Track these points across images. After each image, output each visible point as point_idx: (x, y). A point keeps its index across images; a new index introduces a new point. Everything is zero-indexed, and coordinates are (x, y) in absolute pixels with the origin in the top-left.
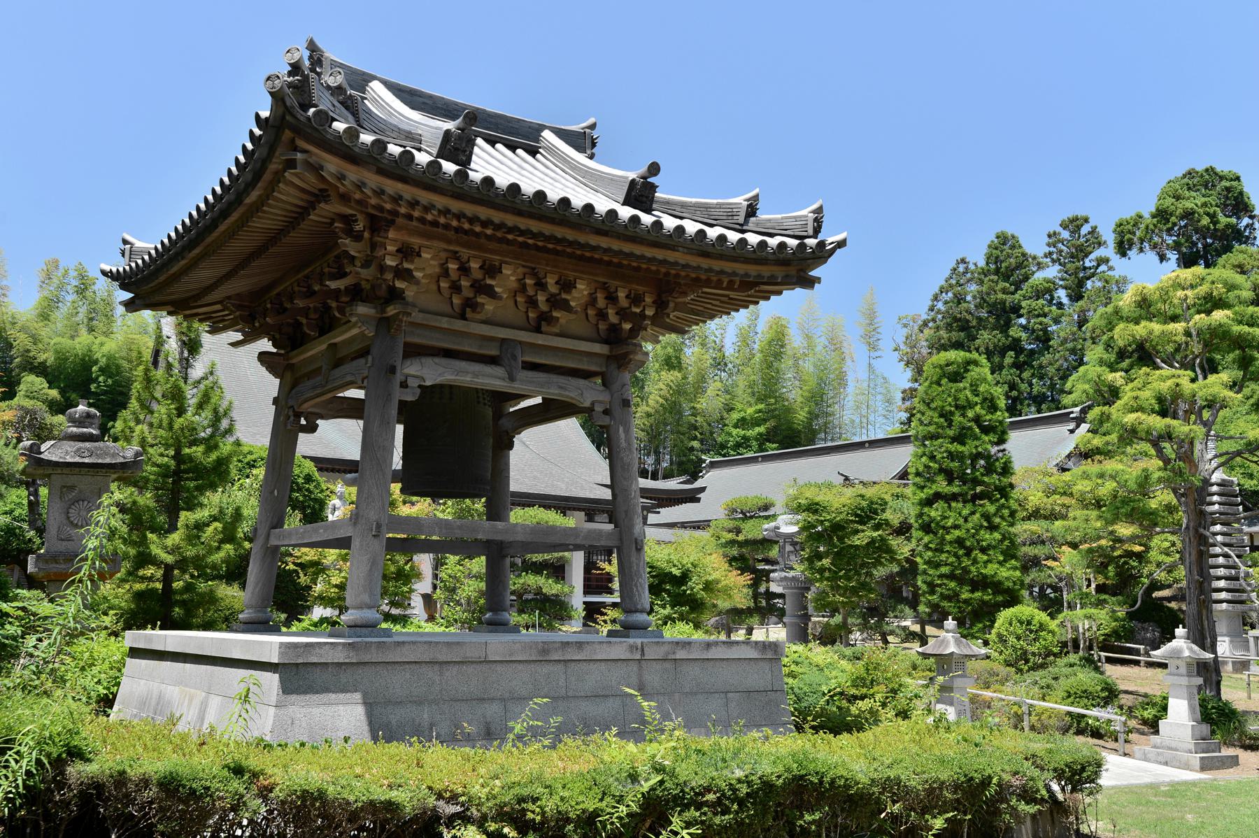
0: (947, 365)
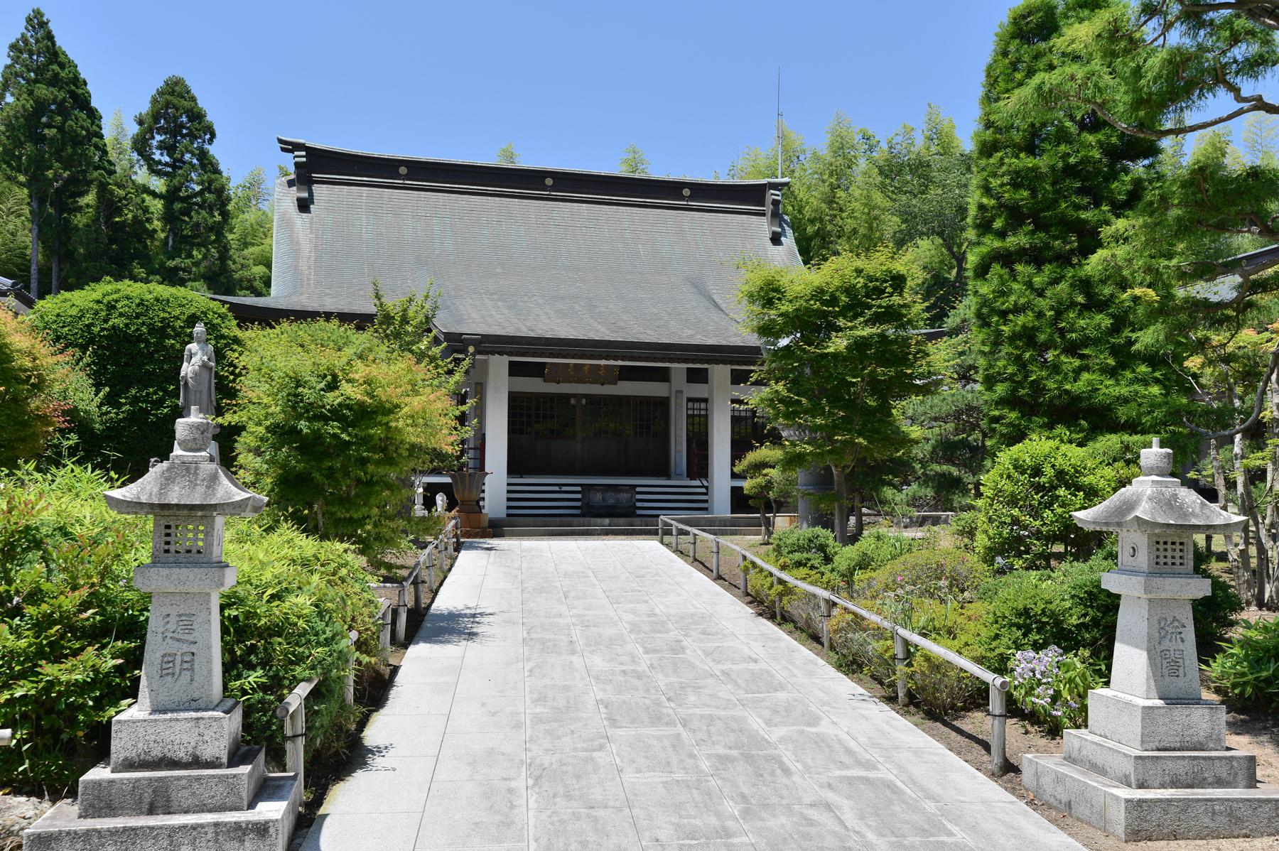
0: (1030, 14)
